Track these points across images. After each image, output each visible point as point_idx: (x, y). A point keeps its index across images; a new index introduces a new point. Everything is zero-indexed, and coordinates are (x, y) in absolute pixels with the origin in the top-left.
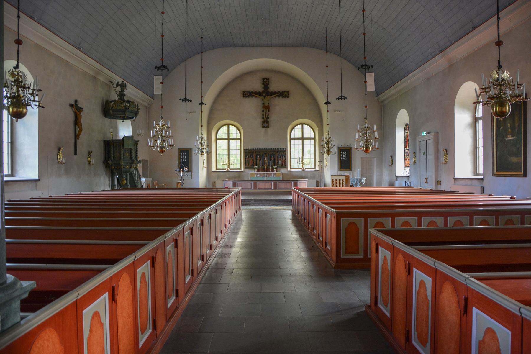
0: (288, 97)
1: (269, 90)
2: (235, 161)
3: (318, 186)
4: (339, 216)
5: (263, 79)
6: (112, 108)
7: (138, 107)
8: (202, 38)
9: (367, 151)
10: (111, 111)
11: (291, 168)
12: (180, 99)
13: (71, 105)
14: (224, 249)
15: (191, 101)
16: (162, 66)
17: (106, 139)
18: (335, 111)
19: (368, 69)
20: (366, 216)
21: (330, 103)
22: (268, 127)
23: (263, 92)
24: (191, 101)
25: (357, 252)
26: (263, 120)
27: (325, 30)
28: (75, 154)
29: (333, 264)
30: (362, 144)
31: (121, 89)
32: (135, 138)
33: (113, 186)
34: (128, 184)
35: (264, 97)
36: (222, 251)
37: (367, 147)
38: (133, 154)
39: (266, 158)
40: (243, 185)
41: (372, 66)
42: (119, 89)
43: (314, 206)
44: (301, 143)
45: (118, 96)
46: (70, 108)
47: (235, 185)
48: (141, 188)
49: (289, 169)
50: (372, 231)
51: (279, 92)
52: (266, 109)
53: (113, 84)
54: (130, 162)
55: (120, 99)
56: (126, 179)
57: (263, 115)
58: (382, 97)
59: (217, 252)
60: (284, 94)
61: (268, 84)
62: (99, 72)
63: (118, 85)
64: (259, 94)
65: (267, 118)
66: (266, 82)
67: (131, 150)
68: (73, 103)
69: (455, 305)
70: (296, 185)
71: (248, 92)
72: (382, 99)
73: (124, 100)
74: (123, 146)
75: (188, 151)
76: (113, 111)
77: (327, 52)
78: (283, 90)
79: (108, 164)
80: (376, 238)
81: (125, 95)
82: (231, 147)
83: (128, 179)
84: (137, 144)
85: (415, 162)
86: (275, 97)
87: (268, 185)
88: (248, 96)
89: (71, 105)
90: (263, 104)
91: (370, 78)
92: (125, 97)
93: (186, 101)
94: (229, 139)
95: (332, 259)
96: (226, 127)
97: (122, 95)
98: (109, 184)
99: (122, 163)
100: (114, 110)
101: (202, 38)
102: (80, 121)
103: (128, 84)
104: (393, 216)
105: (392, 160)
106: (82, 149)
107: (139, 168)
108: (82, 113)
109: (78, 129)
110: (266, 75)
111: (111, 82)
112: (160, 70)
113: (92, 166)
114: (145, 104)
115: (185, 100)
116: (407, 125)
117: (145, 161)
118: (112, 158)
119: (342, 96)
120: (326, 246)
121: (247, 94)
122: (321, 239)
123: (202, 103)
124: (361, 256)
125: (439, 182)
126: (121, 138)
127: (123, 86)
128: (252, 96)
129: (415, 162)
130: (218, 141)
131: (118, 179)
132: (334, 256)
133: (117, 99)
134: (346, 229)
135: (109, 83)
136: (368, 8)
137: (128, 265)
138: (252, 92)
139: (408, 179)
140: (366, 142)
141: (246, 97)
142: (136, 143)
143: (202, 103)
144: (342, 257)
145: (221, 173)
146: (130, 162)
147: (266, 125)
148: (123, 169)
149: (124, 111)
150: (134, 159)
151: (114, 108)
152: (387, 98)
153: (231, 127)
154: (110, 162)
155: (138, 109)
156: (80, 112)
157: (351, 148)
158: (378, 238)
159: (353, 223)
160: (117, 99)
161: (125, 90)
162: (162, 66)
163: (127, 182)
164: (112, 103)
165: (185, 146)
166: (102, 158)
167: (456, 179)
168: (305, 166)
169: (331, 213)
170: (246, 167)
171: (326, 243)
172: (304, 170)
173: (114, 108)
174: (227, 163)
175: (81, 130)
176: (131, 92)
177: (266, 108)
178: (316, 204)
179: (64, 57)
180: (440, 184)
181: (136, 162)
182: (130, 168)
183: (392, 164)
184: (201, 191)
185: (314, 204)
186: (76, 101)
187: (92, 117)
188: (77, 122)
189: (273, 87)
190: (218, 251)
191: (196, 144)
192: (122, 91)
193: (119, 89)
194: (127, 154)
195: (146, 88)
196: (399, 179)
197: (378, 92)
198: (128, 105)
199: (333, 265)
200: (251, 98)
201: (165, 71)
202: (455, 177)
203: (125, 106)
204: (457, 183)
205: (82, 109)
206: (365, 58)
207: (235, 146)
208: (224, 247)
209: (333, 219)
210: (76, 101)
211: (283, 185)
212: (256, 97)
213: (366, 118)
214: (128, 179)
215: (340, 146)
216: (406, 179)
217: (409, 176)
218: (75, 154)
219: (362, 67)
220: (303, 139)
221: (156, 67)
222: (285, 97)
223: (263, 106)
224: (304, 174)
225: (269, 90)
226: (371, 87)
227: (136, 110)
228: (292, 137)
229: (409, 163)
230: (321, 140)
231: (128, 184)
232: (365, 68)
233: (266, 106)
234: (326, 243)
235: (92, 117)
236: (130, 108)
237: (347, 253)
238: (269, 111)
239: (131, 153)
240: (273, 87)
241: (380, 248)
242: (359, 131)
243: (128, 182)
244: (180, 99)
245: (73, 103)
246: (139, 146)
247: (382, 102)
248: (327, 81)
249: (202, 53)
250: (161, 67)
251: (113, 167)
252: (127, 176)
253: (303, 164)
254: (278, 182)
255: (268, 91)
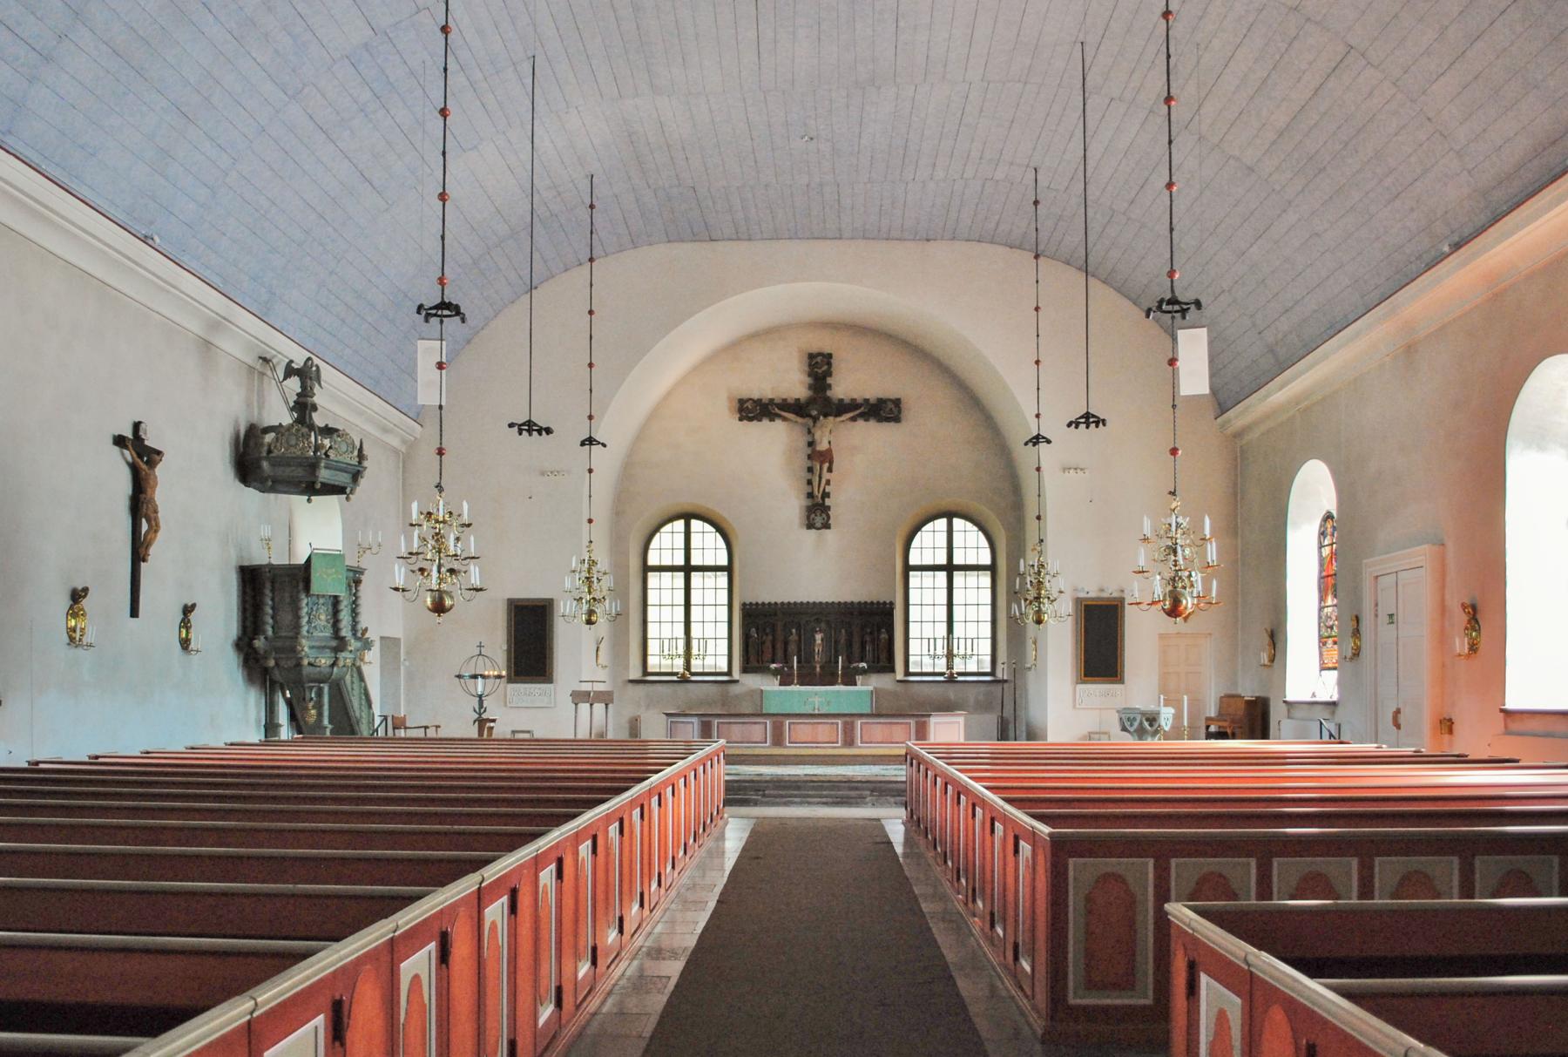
0: (897, 419)
1: (829, 393)
2: (711, 643)
3: (1003, 735)
4: (1060, 849)
5: (811, 356)
6: (269, 451)
7: (361, 450)
8: (592, 207)
9: (1174, 611)
10: (265, 464)
11: (907, 673)
12: (511, 425)
13: (119, 441)
14: (648, 964)
15: (548, 431)
16: (444, 305)
17: (246, 564)
18: (1066, 469)
19: (1184, 312)
20: (1162, 851)
21: (1049, 442)
22: (827, 526)
23: (811, 401)
24: (548, 431)
25: (1126, 982)
26: (809, 502)
27: (1031, 175)
28: (134, 612)
29: (1039, 1025)
30: (1159, 588)
31: (303, 386)
32: (351, 561)
33: (271, 727)
34: (326, 721)
35: (815, 419)
36: (641, 969)
37: (1176, 602)
38: (345, 616)
39: (819, 637)
40: (737, 731)
41: (1198, 304)
42: (294, 384)
43: (979, 810)
44: (945, 584)
45: (292, 409)
46: (116, 449)
47: (706, 732)
48: (372, 738)
49: (900, 675)
50: (1181, 912)
51: (867, 401)
52: (822, 464)
53: (274, 369)
54: (334, 643)
55: (297, 421)
56: (319, 706)
57: (810, 482)
58: (1239, 417)
59: (618, 973)
60: (884, 411)
61: (829, 373)
62: (218, 324)
63: (290, 371)
64: (797, 409)
65: (826, 495)
66: (819, 367)
67: (336, 601)
68: (129, 434)
69: (1456, 953)
70: (921, 733)
71: (758, 402)
72: (1239, 424)
73: (312, 427)
74: (307, 588)
75: (544, 607)
76: (273, 465)
77: (1037, 257)
78: (881, 395)
79: (255, 651)
80: (1192, 942)
81: (314, 408)
82: (696, 597)
83: (326, 707)
84: (358, 582)
85: (1357, 653)
86: (853, 419)
87: (823, 731)
88: (758, 418)
89: (119, 441)
90: (811, 444)
91: (1193, 346)
92: (314, 415)
93: (530, 432)
94: (688, 569)
95: (1034, 1008)
96: (679, 525)
97: (303, 407)
98: (258, 721)
99: (305, 645)
100: (275, 460)
101: (592, 207)
102: (152, 500)
103: (327, 373)
104: (1266, 850)
105: (1274, 645)
106: (160, 594)
107: (365, 668)
108: (159, 470)
109: (145, 527)
110: (821, 342)
111: (265, 360)
112: (434, 321)
113: (195, 658)
114: (395, 442)
115: (529, 427)
116: (1328, 517)
117: (389, 643)
118: (270, 632)
119: (1087, 416)
120: (1016, 959)
121: (754, 410)
122: (1000, 931)
123: (590, 441)
124: (1144, 998)
125: (1447, 725)
126: (303, 561)
127: (306, 375)
128: (772, 417)
129: (1357, 653)
130: (653, 578)
131: (289, 703)
132: (1041, 998)
133: (286, 419)
134: (1089, 899)
135: (258, 365)
136: (1185, 92)
137: (223, 1039)
138: (772, 400)
139: (1333, 713)
140: (1173, 580)
141: (750, 419)
142: (355, 579)
143: (590, 441)
144: (1072, 1001)
145: (659, 687)
146: (334, 643)
147: (819, 521)
148: (307, 670)
149: (313, 466)
150: (346, 632)
151: (275, 453)
152: (1256, 423)
153: (696, 525)
154: (259, 643)
155: (361, 456)
156: (152, 464)
157: (1122, 600)
158: (1195, 942)
159: (1118, 878)
160: (286, 419)
161: (317, 389)
162: (444, 305)
163: (320, 714)
164: (269, 438)
165: (1096, 690)
166: (233, 631)
167: (1508, 713)
168: (959, 666)
169: (1033, 837)
170: (745, 670)
171: (1016, 946)
172: (951, 680)
173: (275, 453)
174: (681, 651)
175: (154, 528)
176: (337, 401)
177: (819, 459)
178: (984, 803)
179: (98, 270)
180: (1451, 731)
181: (354, 644)
182: (333, 665)
183: (1272, 660)
184: (458, 753)
185: (976, 802)
186: (137, 426)
187: (196, 482)
188: (140, 503)
189: (843, 387)
190: (624, 969)
191: (568, 585)
192: (305, 393)
193: (294, 384)
194: (323, 618)
195: (390, 383)
196: (1297, 713)
197: (1222, 400)
198: (327, 442)
199: (1040, 1032)
200: (766, 422)
201: (452, 323)
202: (1510, 704)
203: (317, 448)
204: (1515, 726)
205: (159, 453)
206: (1171, 274)
207: (711, 592)
208: (648, 954)
209: (1041, 859)
210: (137, 426)
211: (878, 729)
212: (785, 419)
213: (1173, 493)
214: (326, 707)
215: (1082, 595)
216: (1321, 714)
217: (1334, 704)
218: (134, 612)
219: (1159, 307)
220: (950, 568)
221: (420, 307)
222: (888, 420)
223: (809, 451)
224: (951, 692)
225: (829, 393)
226: (1194, 379)
227: (355, 461)
228: (912, 562)
229: (1333, 655)
230: (1014, 572)
231: (326, 721)
232: (1174, 309)
233: (821, 454)
234: (1016, 946)
235: (196, 482)
236: (332, 454)
237: (1091, 985)
238: (830, 470)
239: (336, 612)
240: (843, 387)
241: (1204, 979)
242: (1145, 539)
243: (326, 713)
244: (511, 425)
245: (129, 434)
246: (362, 587)
247: (1238, 435)
248: (1037, 362)
249: (591, 260)
250: (436, 307)
251: (272, 663)
252: (320, 694)
253: (950, 656)
254: (859, 722)
255: (828, 400)
